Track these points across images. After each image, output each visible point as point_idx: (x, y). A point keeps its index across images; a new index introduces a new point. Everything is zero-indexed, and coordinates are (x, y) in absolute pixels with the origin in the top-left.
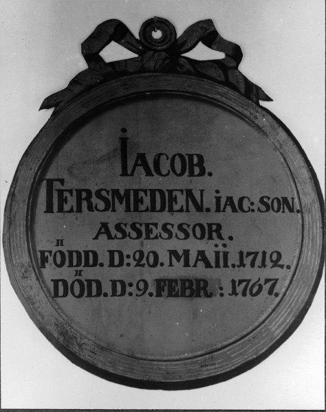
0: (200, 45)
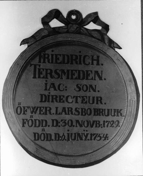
0: (92, 23)
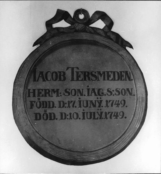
0: (100, 20)
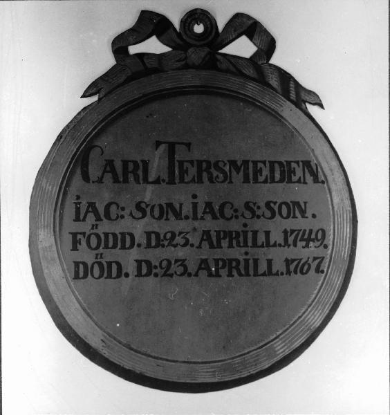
0: (154, 38)
